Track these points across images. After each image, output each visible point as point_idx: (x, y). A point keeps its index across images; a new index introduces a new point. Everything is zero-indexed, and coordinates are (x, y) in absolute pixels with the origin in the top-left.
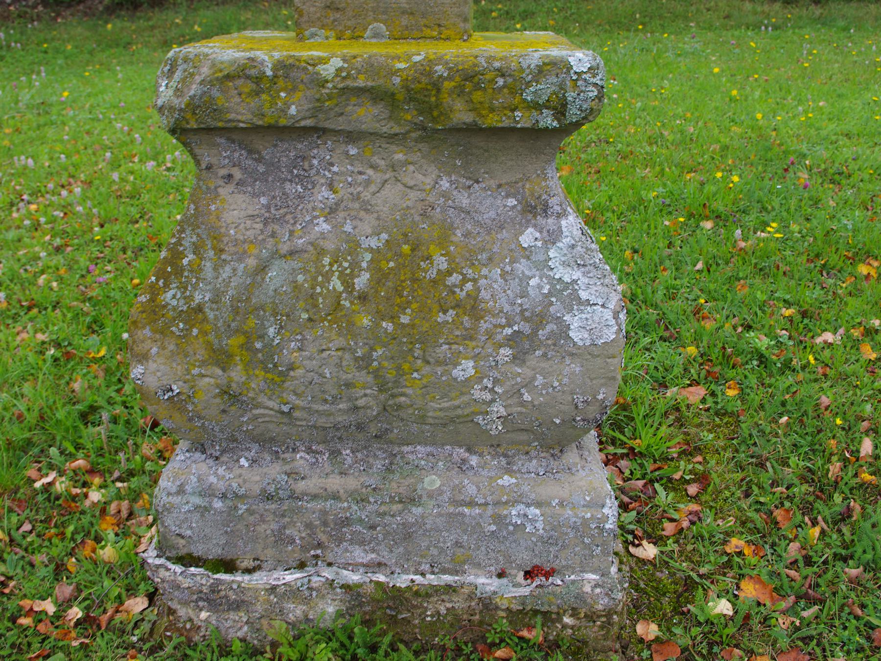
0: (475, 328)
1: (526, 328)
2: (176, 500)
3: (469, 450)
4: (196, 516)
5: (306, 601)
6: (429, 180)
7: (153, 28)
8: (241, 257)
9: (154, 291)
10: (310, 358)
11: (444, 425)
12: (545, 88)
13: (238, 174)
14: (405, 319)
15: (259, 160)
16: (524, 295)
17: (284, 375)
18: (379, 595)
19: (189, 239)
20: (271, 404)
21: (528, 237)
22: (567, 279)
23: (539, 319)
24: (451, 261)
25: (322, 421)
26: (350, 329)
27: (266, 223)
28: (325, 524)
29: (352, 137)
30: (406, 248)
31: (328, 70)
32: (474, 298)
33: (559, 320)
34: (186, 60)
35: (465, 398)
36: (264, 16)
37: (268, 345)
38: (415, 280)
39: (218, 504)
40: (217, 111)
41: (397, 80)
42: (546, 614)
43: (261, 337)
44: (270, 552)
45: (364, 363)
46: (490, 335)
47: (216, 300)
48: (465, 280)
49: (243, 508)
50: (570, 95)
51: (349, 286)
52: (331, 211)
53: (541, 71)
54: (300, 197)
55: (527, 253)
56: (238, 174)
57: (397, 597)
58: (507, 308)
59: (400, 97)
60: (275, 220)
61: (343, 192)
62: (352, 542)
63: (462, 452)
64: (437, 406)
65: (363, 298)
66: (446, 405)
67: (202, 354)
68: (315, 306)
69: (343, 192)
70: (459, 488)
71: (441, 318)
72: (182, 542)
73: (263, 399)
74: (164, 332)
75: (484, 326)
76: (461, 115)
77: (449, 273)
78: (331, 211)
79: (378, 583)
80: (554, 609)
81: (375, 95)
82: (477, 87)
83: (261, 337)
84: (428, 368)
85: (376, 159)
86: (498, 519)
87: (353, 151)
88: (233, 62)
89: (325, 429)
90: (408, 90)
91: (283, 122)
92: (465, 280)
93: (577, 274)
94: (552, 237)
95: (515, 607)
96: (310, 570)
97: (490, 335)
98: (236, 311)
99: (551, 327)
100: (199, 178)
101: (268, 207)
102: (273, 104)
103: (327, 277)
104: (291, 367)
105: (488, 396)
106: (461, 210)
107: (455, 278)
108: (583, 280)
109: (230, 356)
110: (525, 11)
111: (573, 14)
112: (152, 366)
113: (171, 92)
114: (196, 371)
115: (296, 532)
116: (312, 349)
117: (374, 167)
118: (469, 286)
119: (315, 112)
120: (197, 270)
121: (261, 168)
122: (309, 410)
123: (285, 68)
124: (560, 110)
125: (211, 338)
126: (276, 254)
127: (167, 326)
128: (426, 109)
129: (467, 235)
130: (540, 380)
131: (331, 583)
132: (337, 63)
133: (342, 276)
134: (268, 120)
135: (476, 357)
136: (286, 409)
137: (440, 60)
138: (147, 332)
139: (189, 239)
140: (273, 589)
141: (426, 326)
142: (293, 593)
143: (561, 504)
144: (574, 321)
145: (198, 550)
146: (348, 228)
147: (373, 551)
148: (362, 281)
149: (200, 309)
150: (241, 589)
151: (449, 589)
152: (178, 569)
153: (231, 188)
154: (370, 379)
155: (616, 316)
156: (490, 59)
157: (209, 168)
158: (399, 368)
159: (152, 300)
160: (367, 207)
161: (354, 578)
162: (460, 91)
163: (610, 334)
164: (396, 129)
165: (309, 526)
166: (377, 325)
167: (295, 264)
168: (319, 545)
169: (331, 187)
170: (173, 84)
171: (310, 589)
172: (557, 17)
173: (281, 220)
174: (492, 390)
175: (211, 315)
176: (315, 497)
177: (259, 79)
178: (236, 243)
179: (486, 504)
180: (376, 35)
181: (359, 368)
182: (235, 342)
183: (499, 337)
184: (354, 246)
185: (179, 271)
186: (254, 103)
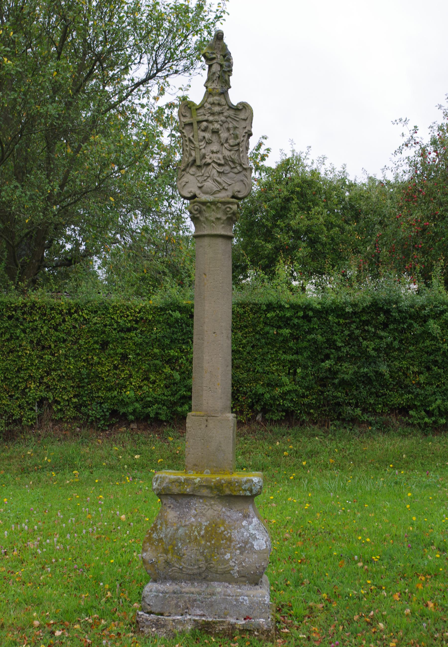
0: (230, 545)
1: (243, 545)
2: (149, 593)
3: (229, 584)
4: (154, 598)
5: (183, 624)
6: (220, 509)
7: (10, 458)
8: (172, 526)
9: (150, 534)
10: (189, 552)
11: (222, 574)
12: (247, 486)
13: (172, 506)
14: (213, 542)
15: (178, 503)
16: (243, 536)
17: (181, 557)
18: (203, 623)
19: (159, 522)
20: (177, 566)
21: (244, 523)
22: (253, 533)
23: (246, 543)
24: (225, 528)
25: (190, 572)
26: (199, 544)
27: (179, 518)
28: (189, 601)
29: (201, 497)
30: (214, 525)
31: (197, 481)
32: (230, 537)
33: (251, 543)
34: (161, 478)
35: (228, 565)
36: (100, 451)
37: (178, 548)
38: (216, 533)
39: (161, 595)
40: (170, 490)
41: (213, 484)
42: (250, 631)
43: (177, 546)
44: (173, 611)
45: (202, 554)
46: (234, 547)
47: (166, 536)
48: (228, 533)
49: (167, 595)
50: (253, 488)
51: (199, 534)
52: (195, 516)
53: (246, 482)
54: (187, 512)
55: (244, 527)
56: (172, 506)
57: (208, 623)
58: (238, 540)
59: (213, 488)
60: (181, 518)
61: (198, 511)
62: (196, 607)
63: (227, 584)
64: (221, 568)
65: (203, 537)
66: (223, 567)
67: (161, 550)
68: (191, 538)
69: (198, 511)
70: (226, 591)
71: (222, 542)
72: (149, 607)
73: (175, 564)
74: (152, 544)
75: (232, 544)
76: (228, 492)
77: (224, 531)
78: (195, 516)
79: (203, 620)
80: (252, 629)
81: (207, 487)
82: (231, 485)
83: (177, 546)
84: (218, 556)
85: (207, 503)
86: (237, 600)
87: (201, 501)
88: (174, 479)
89: (190, 575)
90: (215, 486)
91: (185, 493)
92: (228, 533)
93: (256, 532)
94: (250, 523)
95: (241, 628)
96: (184, 616)
97: (234, 547)
98: (171, 539)
99: (249, 545)
100: (162, 507)
101: (179, 515)
102: (183, 488)
103: (194, 531)
104: (184, 555)
105: (234, 564)
106: (228, 516)
107: (226, 532)
108: (257, 533)
109: (168, 551)
110: (311, 451)
111: (351, 454)
112: (148, 553)
113: (157, 485)
114: (159, 555)
115: (181, 604)
116: (189, 550)
117: (206, 505)
118: (229, 534)
119: (193, 491)
120: (161, 529)
121: (178, 505)
122: (187, 569)
123: (187, 480)
124: (251, 491)
125: (164, 546)
126: (181, 526)
127: (153, 543)
128: (219, 490)
129: (229, 522)
130: (247, 560)
131: (190, 619)
132: (199, 479)
133: (197, 531)
134: (182, 492)
135: (231, 553)
136: (181, 567)
137: (223, 479)
138: (148, 544)
139: (159, 522)
140: (174, 620)
141: (218, 544)
142: (179, 622)
143: (253, 596)
144: (255, 543)
145: (154, 610)
146: (199, 520)
147: (202, 610)
148: (202, 533)
149: (162, 539)
150: (166, 620)
151: (223, 622)
152: (148, 615)
153: (170, 509)
154: (203, 558)
155: (266, 542)
156: (234, 479)
157: (165, 504)
158: (211, 555)
159: (150, 536)
160: (204, 515)
161: (197, 618)
162: (227, 486)
163: (264, 547)
164: (212, 496)
165: (185, 602)
166: (206, 543)
167: (186, 528)
168: (187, 608)
169: (195, 510)
170: (158, 483)
171: (184, 621)
172: (337, 456)
173: (182, 518)
174: (235, 562)
175: (164, 540)
176: (187, 593)
177: (180, 483)
178: (171, 523)
179: (233, 596)
180: (207, 473)
181: (201, 555)
182: (170, 547)
183: (236, 547)
184: (201, 524)
185: (156, 529)
186: (179, 488)
